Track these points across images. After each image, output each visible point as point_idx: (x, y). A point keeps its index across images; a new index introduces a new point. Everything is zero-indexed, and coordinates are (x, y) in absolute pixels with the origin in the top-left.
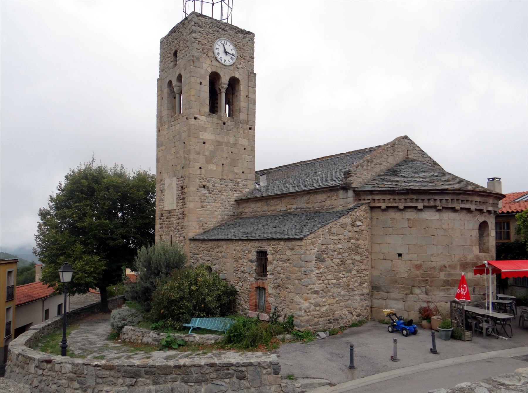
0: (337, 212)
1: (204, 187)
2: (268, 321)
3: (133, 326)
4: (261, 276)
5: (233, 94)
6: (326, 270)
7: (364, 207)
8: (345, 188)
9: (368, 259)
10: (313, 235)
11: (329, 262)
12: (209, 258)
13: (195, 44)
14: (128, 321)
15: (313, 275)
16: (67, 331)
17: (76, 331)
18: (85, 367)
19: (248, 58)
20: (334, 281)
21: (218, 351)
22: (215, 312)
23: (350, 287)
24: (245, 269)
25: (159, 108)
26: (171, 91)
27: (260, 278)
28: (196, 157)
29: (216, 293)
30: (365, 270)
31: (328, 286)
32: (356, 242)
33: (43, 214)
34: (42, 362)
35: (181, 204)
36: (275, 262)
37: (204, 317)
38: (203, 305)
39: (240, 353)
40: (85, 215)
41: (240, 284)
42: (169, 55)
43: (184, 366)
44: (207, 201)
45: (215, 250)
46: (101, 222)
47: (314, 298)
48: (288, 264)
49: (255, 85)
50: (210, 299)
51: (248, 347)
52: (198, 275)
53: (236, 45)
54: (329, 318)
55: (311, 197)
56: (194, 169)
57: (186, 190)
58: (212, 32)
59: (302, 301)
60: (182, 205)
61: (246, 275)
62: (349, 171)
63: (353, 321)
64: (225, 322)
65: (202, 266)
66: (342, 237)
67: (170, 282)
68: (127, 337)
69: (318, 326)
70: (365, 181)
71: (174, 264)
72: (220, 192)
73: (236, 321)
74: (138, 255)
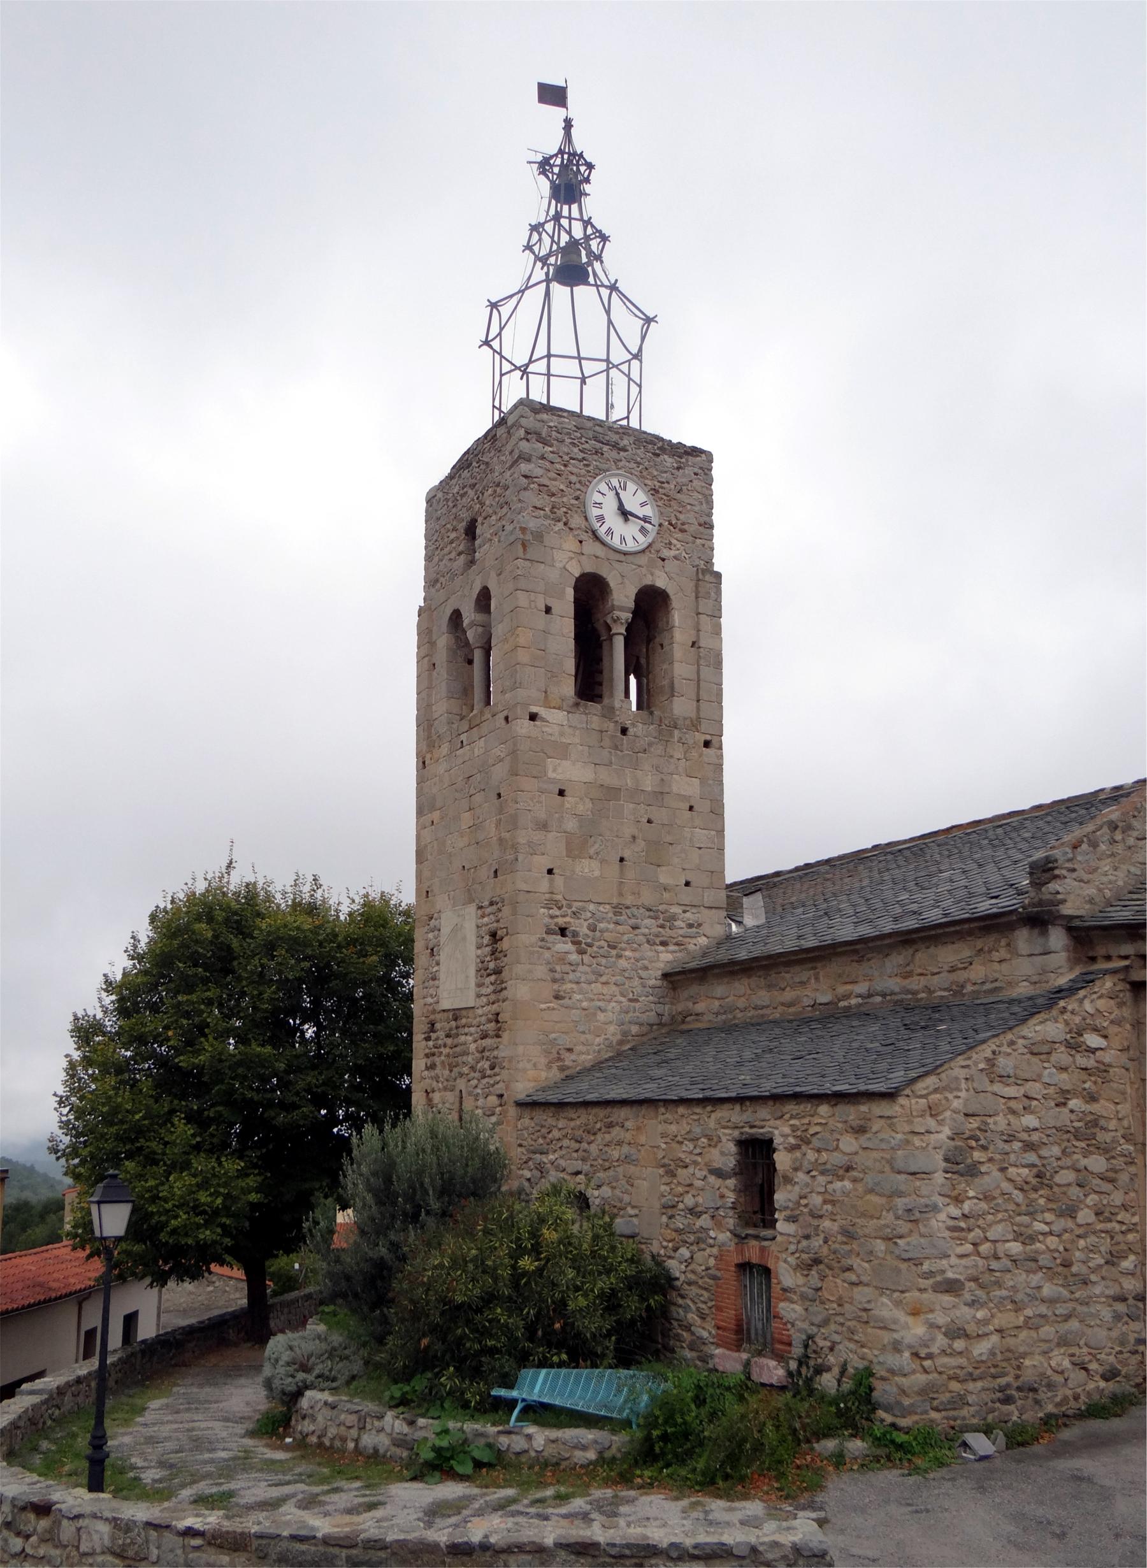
0: (1011, 1002)
1: (563, 932)
2: (783, 1388)
3: (334, 1390)
4: (755, 1226)
5: (649, 640)
6: (984, 1205)
7: (1108, 984)
8: (1038, 919)
9: (1132, 1169)
10: (931, 1081)
11: (992, 1178)
12: (578, 1165)
13: (527, 493)
14: (316, 1372)
15: (939, 1222)
16: (109, 1403)
17: (164, 1401)
18: (153, 1534)
19: (693, 528)
20: (1015, 1248)
21: (609, 1492)
22: (599, 1350)
23: (1074, 1269)
24: (700, 1200)
25: (424, 694)
26: (460, 647)
27: (751, 1231)
28: (537, 836)
29: (603, 1283)
30: (1124, 1207)
31: (994, 1265)
32: (1088, 1108)
33: (85, 1031)
34: (23, 1509)
35: (492, 988)
36: (801, 1176)
37: (561, 1365)
38: (557, 1326)
39: (685, 1502)
40: (202, 1028)
41: (684, 1252)
42: (453, 535)
43: (485, 1547)
44: (571, 976)
45: (599, 1136)
46: (248, 1050)
47: (947, 1310)
48: (847, 1184)
49: (720, 610)
50: (582, 1302)
51: (713, 1482)
52: (542, 1221)
53: (654, 491)
54: (1002, 1381)
55: (919, 955)
56: (529, 877)
57: (505, 945)
58: (581, 456)
59: (902, 1317)
60: (494, 992)
61: (704, 1221)
62: (1048, 860)
63: (1089, 1394)
64: (633, 1386)
65: (556, 1190)
66: (1035, 1088)
67: (450, 1242)
68: (312, 1428)
69: (964, 1412)
70: (1108, 893)
71: (466, 1183)
72: (614, 948)
73: (669, 1384)
74: (355, 1153)
